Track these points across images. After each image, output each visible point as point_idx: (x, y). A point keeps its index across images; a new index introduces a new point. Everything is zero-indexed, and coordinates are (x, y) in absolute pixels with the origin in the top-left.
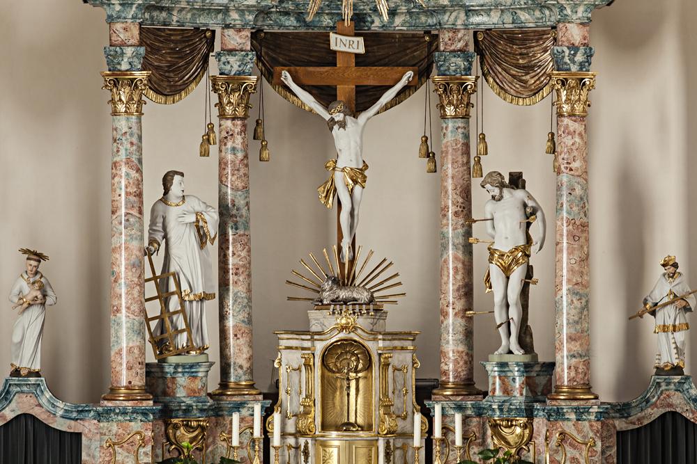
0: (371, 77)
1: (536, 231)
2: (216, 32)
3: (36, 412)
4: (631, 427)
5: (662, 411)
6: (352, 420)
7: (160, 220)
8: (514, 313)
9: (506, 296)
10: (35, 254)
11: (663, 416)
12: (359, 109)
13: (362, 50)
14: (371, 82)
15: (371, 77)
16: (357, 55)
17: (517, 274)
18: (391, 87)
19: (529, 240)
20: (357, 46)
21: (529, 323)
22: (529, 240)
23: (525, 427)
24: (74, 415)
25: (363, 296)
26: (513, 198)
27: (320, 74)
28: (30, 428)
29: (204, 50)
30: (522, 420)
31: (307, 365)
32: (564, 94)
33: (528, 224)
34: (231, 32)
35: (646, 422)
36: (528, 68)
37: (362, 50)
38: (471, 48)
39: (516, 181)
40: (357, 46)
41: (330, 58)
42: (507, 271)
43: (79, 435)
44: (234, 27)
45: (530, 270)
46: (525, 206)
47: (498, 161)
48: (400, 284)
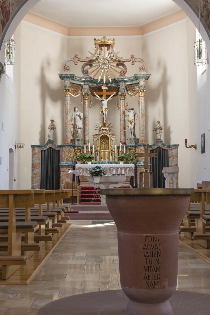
0: (108, 93)
1: (136, 117)
2: (188, 140)
3: (53, 147)
4: (152, 149)
5: (158, 146)
6: (81, 183)
7: (73, 115)
8: (133, 130)
9: (131, 128)
10: (52, 120)
11: (158, 147)
12: (61, 77)
13: (107, 89)
14: (109, 94)
15: (108, 93)
16: (106, 90)
17: (133, 124)
18: (111, 95)
19: (135, 118)
20: (107, 88)
21: (135, 133)
22: (135, 118)
23: (134, 149)
24: (59, 147)
25: (107, 129)
26: (132, 112)
27: (100, 93)
28: (52, 150)
29: (81, 89)
30: (134, 148)
31: (98, 140)
32: (140, 93)
33: (135, 116)
34: (85, 85)
35: (155, 148)
36: (135, 91)
37: (107, 89)
38: (125, 88)
39: (133, 109)
40: (107, 88)
41: (102, 90)
42: (131, 123)
43: (60, 151)
44: (86, 85)
45: (135, 124)
46: (134, 113)
47: (129, 107)
48: (8, 216)
